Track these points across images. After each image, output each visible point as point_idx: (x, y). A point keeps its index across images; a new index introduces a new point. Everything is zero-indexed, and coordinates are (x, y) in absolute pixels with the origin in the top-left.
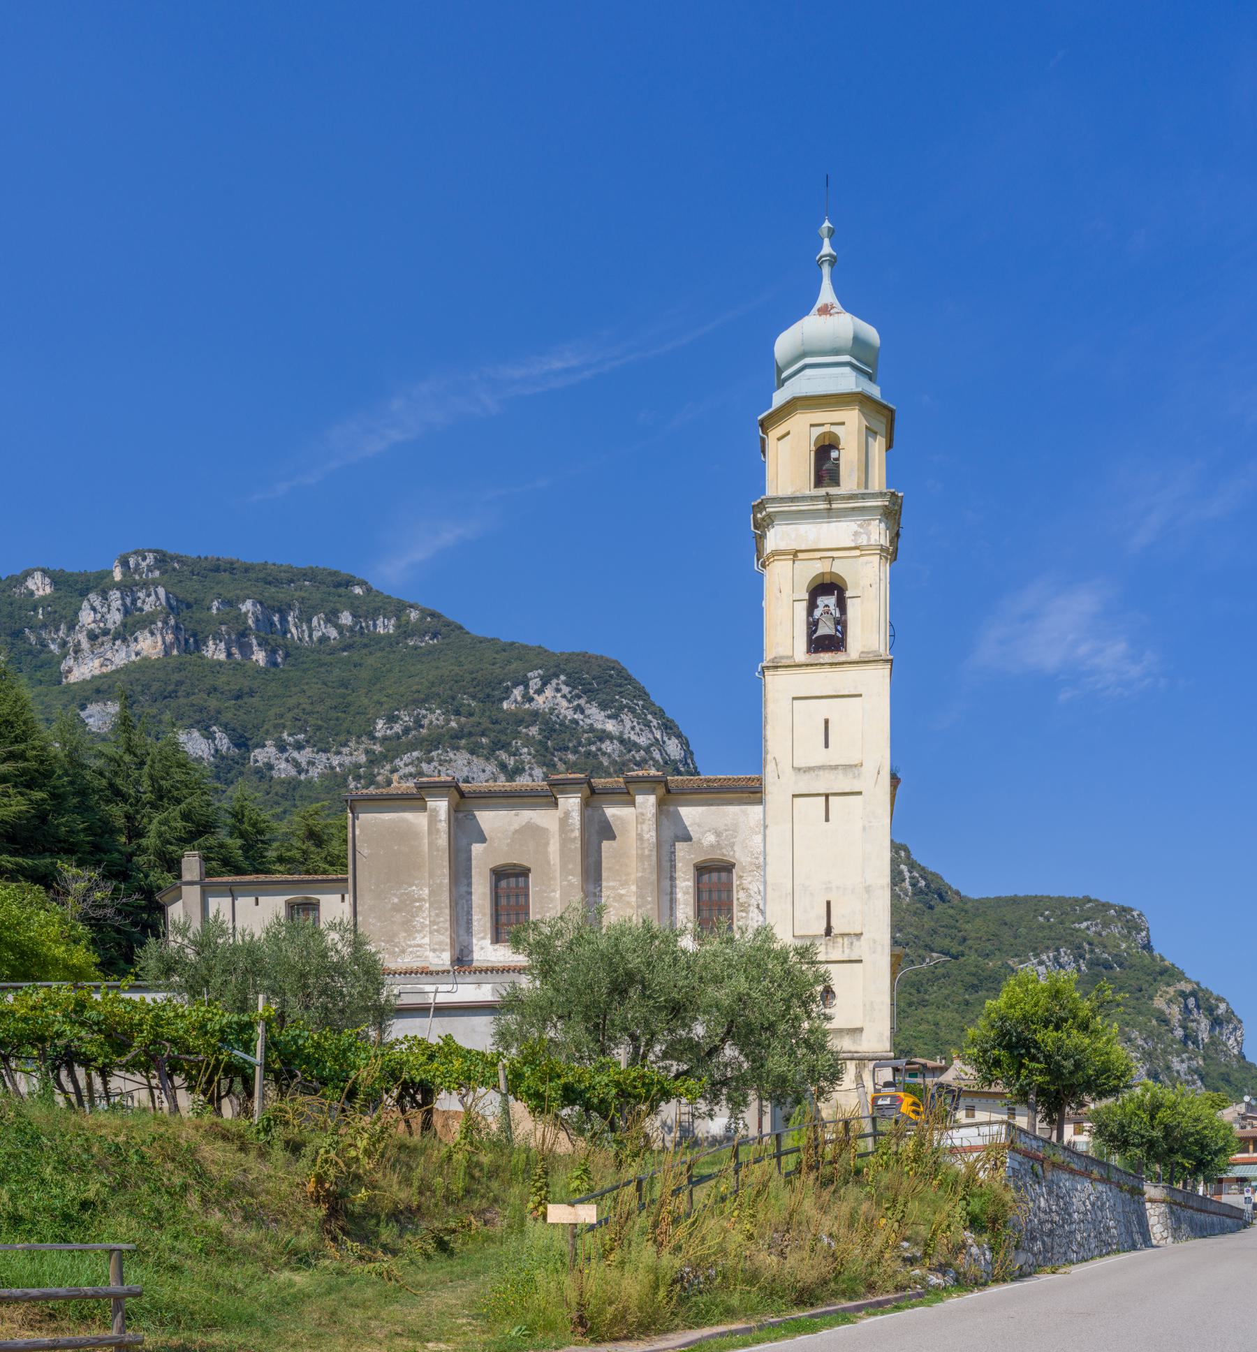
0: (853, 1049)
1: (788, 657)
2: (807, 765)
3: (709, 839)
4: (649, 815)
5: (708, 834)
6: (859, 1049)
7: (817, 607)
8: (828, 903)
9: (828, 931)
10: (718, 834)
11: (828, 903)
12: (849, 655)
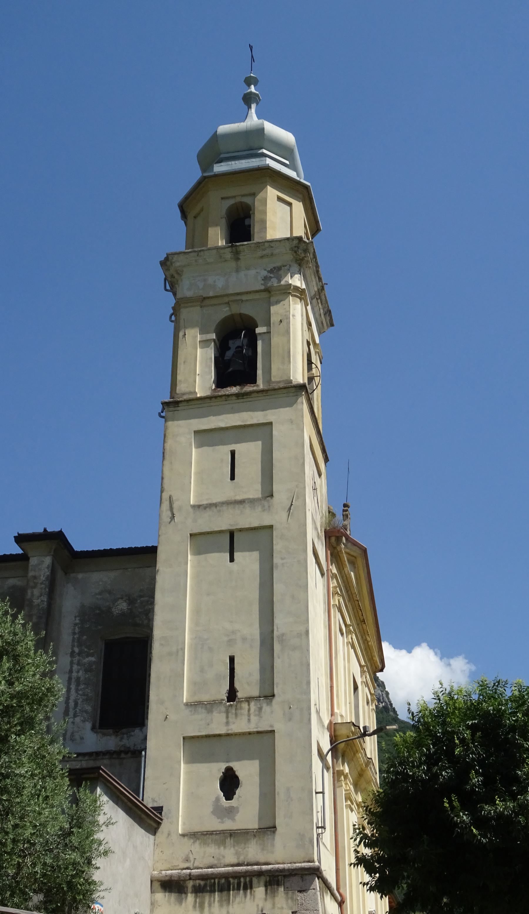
0: (262, 860)
1: (190, 393)
2: (210, 502)
3: (120, 607)
4: (43, 578)
5: (120, 601)
6: (270, 858)
7: (229, 348)
8: (232, 659)
9: (232, 695)
10: (131, 601)
11: (232, 659)
12: (258, 386)
